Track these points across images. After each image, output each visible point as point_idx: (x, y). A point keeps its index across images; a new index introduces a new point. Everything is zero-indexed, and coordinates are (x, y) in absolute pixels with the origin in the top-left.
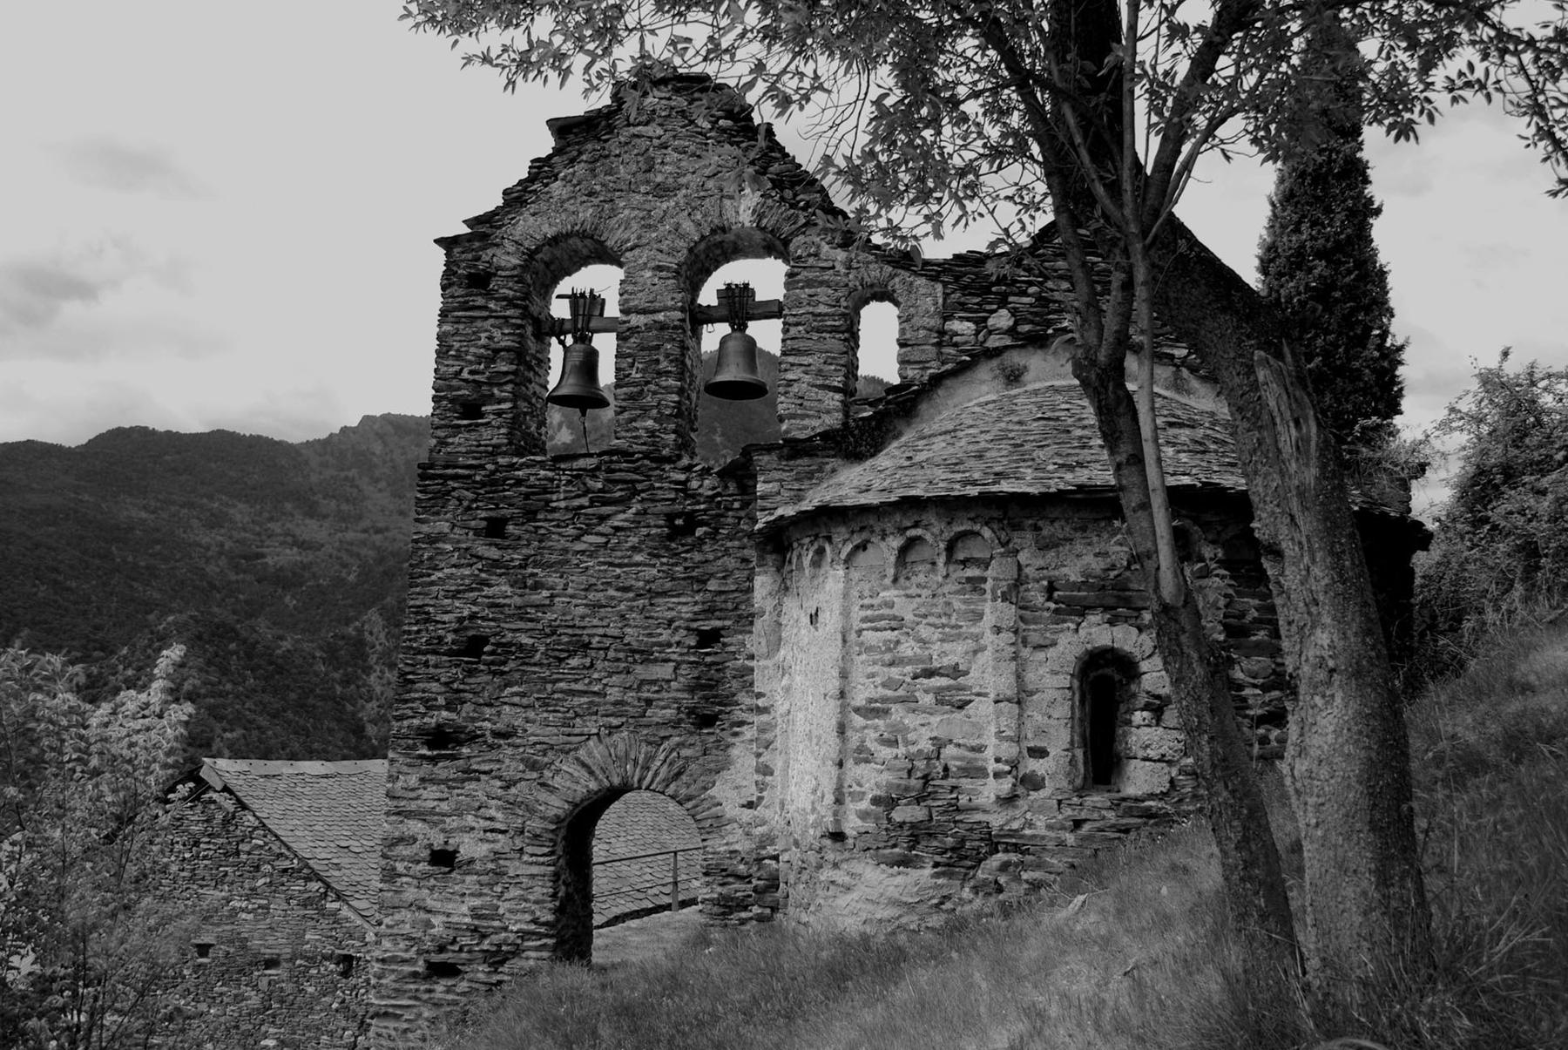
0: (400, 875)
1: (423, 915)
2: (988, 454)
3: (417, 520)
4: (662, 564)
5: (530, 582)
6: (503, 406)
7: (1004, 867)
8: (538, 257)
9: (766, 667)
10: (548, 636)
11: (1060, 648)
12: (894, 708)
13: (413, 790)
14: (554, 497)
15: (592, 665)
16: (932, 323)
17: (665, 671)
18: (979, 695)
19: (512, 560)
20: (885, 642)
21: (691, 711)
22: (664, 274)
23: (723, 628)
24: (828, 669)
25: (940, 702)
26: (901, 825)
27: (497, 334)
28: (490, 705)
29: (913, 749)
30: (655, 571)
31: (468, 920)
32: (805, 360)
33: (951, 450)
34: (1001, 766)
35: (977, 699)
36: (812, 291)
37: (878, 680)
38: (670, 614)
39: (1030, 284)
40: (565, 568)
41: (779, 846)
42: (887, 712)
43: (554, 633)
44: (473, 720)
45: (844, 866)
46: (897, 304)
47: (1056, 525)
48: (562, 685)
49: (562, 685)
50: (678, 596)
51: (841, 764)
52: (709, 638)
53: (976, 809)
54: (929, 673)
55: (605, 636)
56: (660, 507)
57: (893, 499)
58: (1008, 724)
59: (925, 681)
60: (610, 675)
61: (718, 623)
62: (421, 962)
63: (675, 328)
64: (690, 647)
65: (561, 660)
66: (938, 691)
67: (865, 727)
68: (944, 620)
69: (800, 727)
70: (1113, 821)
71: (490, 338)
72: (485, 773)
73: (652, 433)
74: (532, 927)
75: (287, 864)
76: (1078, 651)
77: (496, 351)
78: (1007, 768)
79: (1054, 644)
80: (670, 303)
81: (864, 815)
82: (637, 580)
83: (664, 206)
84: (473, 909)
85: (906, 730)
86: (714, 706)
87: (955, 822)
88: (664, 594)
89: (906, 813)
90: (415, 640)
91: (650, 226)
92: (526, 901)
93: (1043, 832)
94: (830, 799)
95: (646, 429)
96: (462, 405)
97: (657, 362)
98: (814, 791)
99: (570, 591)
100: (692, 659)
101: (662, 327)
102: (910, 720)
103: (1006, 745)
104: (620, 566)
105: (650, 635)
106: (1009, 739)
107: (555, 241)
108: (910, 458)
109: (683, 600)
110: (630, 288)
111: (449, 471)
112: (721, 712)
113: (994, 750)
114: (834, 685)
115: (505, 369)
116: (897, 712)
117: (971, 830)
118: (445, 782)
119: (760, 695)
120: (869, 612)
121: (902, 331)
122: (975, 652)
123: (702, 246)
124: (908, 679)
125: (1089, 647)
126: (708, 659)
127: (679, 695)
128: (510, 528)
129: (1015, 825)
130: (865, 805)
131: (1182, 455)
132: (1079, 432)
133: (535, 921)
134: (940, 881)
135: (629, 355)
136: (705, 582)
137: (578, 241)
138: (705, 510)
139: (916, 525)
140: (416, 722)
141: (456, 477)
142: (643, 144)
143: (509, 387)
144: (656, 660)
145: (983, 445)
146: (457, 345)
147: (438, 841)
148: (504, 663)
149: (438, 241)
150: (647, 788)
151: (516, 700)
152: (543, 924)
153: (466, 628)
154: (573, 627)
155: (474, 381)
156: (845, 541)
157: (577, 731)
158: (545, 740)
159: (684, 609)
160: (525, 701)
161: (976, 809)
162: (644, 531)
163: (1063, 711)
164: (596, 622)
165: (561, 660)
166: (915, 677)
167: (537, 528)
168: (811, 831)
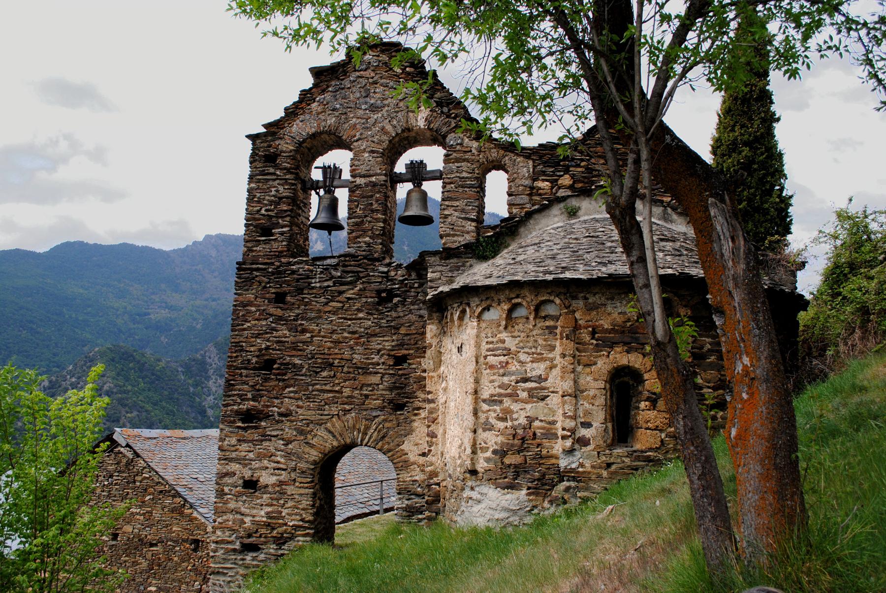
0: (226, 494)
1: (239, 517)
2: (558, 257)
4: (374, 318)
5: (299, 329)
6: (284, 229)
9: (432, 377)
10: (310, 359)
12: (505, 399)
13: (233, 446)
14: (313, 281)
17: (375, 379)
18: (553, 392)
19: (290, 316)
20: (500, 363)
22: (375, 155)
23: (409, 355)
24: (468, 378)
25: (531, 396)
26: (509, 466)
27: (281, 188)
28: (277, 398)
29: (516, 423)
30: (370, 323)
31: (264, 519)
34: (565, 433)
37: (496, 384)
39: (582, 160)
42: (501, 402)
43: (313, 357)
44: (268, 406)
45: (477, 489)
46: (507, 172)
47: (597, 296)
48: (318, 387)
49: (318, 387)
50: (383, 336)
51: (475, 432)
54: (525, 380)
59: (523, 385)
61: (406, 352)
62: (238, 543)
64: (390, 366)
65: (317, 373)
66: (530, 390)
67: (489, 411)
68: (533, 350)
72: (274, 436)
73: (368, 245)
77: (281, 198)
78: (569, 434)
79: (595, 364)
80: (379, 171)
81: (488, 460)
83: (375, 117)
84: (267, 513)
85: (511, 412)
87: (540, 464)
88: (375, 335)
93: (589, 469)
94: (469, 451)
95: (365, 242)
96: (262, 229)
98: (460, 447)
99: (322, 334)
100: (391, 372)
101: (374, 185)
102: (515, 407)
103: (568, 420)
104: (350, 319)
105: (367, 359)
106: (570, 417)
108: (514, 259)
109: (386, 339)
110: (356, 163)
111: (254, 266)
112: (407, 402)
113: (561, 424)
114: (470, 387)
116: (507, 402)
117: (549, 468)
118: (252, 441)
119: (429, 393)
120: (491, 346)
121: (510, 188)
122: (551, 368)
123: (397, 139)
124: (513, 384)
127: (384, 392)
128: (288, 298)
129: (574, 466)
130: (489, 454)
131: (668, 257)
132: (609, 244)
135: (356, 201)
140: (235, 407)
141: (257, 270)
143: (288, 219)
144: (371, 373)
145: (555, 251)
147: (247, 474)
148: (285, 374)
149: (248, 137)
152: (307, 522)
153: (264, 355)
155: (268, 215)
156: (477, 306)
157: (326, 413)
158: (308, 417)
162: (364, 300)
163: (601, 401)
164: (336, 351)
165: (317, 373)
166: (517, 382)
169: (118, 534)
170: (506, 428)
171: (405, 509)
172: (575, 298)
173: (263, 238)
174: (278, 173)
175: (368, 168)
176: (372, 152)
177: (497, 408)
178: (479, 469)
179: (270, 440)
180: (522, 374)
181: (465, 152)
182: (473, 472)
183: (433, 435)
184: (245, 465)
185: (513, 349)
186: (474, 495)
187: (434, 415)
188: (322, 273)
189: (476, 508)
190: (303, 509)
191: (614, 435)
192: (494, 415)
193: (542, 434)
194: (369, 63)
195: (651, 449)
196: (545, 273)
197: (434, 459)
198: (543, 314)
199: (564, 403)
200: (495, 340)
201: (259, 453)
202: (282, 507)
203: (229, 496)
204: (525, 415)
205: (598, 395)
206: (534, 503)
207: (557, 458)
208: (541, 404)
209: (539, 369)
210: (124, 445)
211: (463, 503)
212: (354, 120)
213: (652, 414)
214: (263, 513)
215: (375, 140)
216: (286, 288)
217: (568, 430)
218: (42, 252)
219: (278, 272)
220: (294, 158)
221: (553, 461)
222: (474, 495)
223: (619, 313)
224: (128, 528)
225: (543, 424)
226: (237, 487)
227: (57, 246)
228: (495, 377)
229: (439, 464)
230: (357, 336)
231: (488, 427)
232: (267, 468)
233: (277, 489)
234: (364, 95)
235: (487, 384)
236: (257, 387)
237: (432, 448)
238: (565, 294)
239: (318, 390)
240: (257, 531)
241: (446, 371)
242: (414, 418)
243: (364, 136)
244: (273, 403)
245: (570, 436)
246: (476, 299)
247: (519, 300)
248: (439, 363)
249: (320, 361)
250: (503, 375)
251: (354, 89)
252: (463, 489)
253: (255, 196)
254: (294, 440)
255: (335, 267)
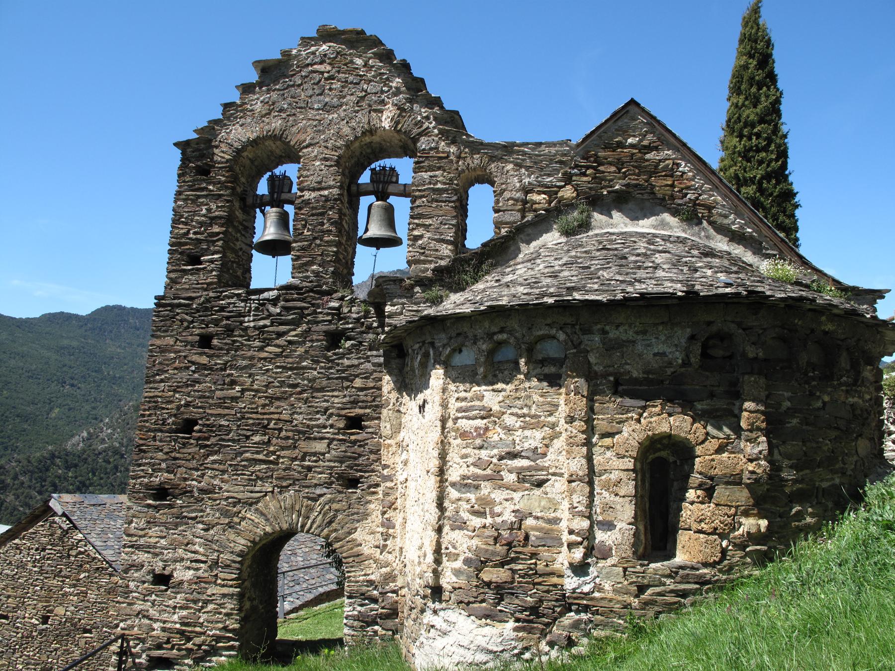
0: (132, 592)
1: (147, 621)
2: (561, 275)
3: (153, 336)
4: (321, 368)
5: (227, 380)
6: (215, 256)
7: (576, 625)
8: (245, 154)
9: (390, 446)
10: (240, 420)
11: (625, 434)
12: (483, 484)
13: (142, 530)
14: (246, 319)
15: (269, 441)
16: (518, 195)
17: (321, 446)
18: (554, 474)
19: (216, 364)
20: (477, 429)
21: (340, 477)
22: (328, 163)
23: (364, 415)
24: (430, 450)
25: (521, 480)
26: (488, 584)
27: (213, 206)
28: (197, 470)
29: (499, 520)
30: (315, 373)
31: (178, 626)
32: (428, 222)
33: (531, 273)
34: (574, 538)
35: (553, 478)
36: (431, 174)
37: (470, 460)
38: (325, 404)
39: (588, 168)
40: (253, 371)
41: (399, 583)
42: (477, 487)
43: (243, 418)
44: (185, 479)
45: (441, 613)
46: (492, 184)
47: (621, 329)
48: (248, 455)
49: (248, 455)
50: (333, 390)
51: (439, 530)
52: (355, 423)
53: (552, 574)
54: (513, 455)
55: (279, 420)
56: (322, 327)
57: (482, 308)
58: (579, 499)
59: (509, 462)
60: (283, 448)
61: (361, 411)
62: (144, 656)
63: (335, 200)
64: (339, 429)
65: (248, 437)
66: (519, 471)
67: (459, 500)
68: (525, 411)
69: (411, 493)
70: (672, 587)
71: (209, 210)
72: (192, 518)
73: (317, 274)
74: (222, 634)
75: (99, 565)
76: (642, 436)
77: (212, 219)
78: (579, 539)
79: (620, 432)
80: (332, 183)
81: (457, 572)
82: (303, 379)
83: (330, 117)
84: (181, 618)
85: (492, 503)
86: (356, 475)
87: (534, 584)
88: (322, 390)
89: (491, 574)
90: (147, 421)
91: (319, 131)
92: (219, 615)
93: (610, 595)
94: (430, 558)
95: (313, 272)
96: (188, 256)
97: (322, 224)
98: (420, 548)
99: (255, 387)
100: (341, 437)
101: (327, 199)
102: (498, 495)
103: (578, 519)
104: (291, 369)
105: (310, 419)
106: (582, 515)
107: (255, 143)
108: (497, 281)
109: (336, 393)
110: (305, 173)
111: (176, 301)
112: (362, 477)
113: (570, 523)
114: (434, 464)
115: (217, 230)
116: (486, 489)
117: (548, 592)
118: (164, 524)
119: (385, 467)
120: (463, 404)
121: (497, 202)
122: (552, 439)
123: (357, 144)
124: (495, 460)
125: (650, 433)
126: (353, 438)
127: (332, 464)
128: (215, 342)
129: (586, 589)
130: (458, 564)
131: (719, 275)
132: (633, 258)
133: (225, 629)
134: (520, 634)
135: (303, 220)
136: (352, 381)
137: (271, 143)
138: (352, 329)
139: (502, 331)
140: (146, 480)
141: (179, 305)
142: (317, 77)
143: (220, 243)
144: (315, 439)
145: (557, 268)
146: (186, 215)
147: (158, 566)
148: (207, 439)
149: (175, 144)
150: (308, 532)
151: (216, 466)
152: (230, 631)
153: (183, 413)
154: (257, 413)
155: (196, 239)
156: (444, 346)
157: (257, 489)
158: (235, 495)
159: (336, 400)
160: (221, 467)
161: (552, 574)
162: (308, 344)
163: (629, 488)
164: (272, 410)
165: (248, 437)
166: (501, 458)
167: (234, 341)
168: (418, 580)
169: (48, 617)
170: (484, 527)
171: (356, 618)
172: (587, 331)
173: (189, 267)
174: (211, 187)
175: (319, 179)
176: (326, 159)
177: (472, 496)
178: (445, 585)
179: (187, 524)
180: (507, 446)
181: (441, 158)
182: (436, 592)
183: (388, 524)
184: (156, 555)
185: (496, 408)
186: (437, 621)
187: (391, 498)
188: (257, 309)
189: (440, 642)
190: (227, 615)
191: (646, 539)
192: (465, 506)
193: (537, 538)
194: (325, 55)
195: (705, 565)
196: (543, 295)
197: (390, 557)
198: (540, 357)
199: (571, 492)
200: (468, 395)
201: (174, 540)
202: (199, 611)
203: (135, 594)
204: (513, 507)
205: (625, 479)
206: (525, 644)
207: (561, 576)
208: (537, 492)
209: (534, 438)
210: (60, 513)
211: (423, 632)
212: (304, 122)
213: (708, 509)
214: (175, 617)
215: (329, 145)
216: (212, 329)
217: (578, 534)
218: (84, 314)
219: (205, 308)
220: (231, 169)
221: (555, 580)
222: (437, 621)
223: (655, 355)
224: (60, 610)
225: (541, 523)
226: (144, 582)
227: (98, 310)
228: (469, 451)
229: (397, 566)
230: (299, 389)
231: (461, 525)
232: (182, 560)
233: (194, 586)
234: (317, 92)
235: (458, 460)
236: (173, 455)
237: (388, 542)
238: (573, 326)
239: (247, 460)
240: (168, 642)
241: (406, 438)
242: (369, 498)
243: (316, 141)
244: (192, 475)
245: (581, 543)
246: (443, 336)
247: (504, 336)
248: (398, 428)
249: (251, 421)
250: (481, 448)
251: (305, 86)
252: (423, 611)
253: (182, 216)
254: (217, 524)
255: (274, 302)
